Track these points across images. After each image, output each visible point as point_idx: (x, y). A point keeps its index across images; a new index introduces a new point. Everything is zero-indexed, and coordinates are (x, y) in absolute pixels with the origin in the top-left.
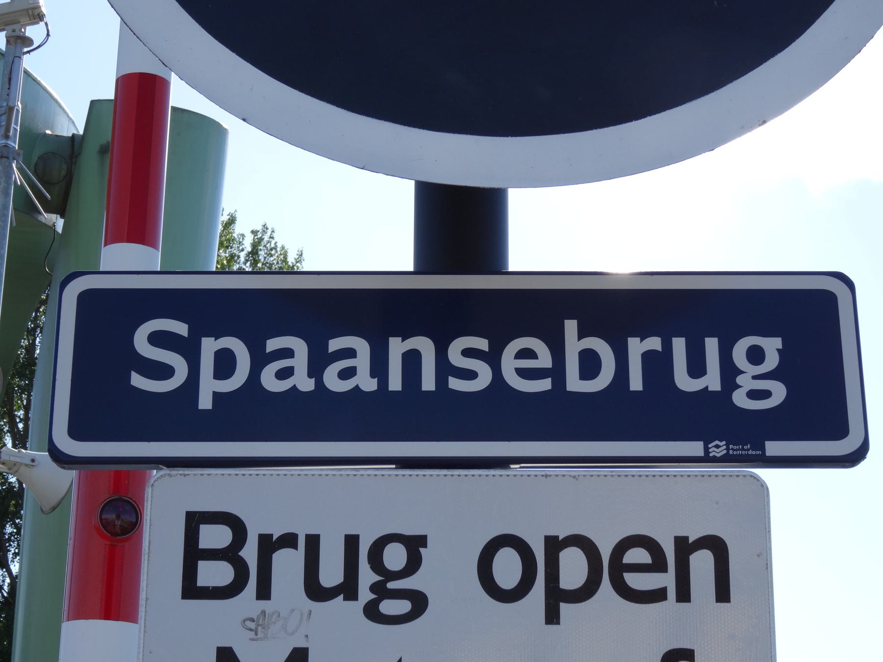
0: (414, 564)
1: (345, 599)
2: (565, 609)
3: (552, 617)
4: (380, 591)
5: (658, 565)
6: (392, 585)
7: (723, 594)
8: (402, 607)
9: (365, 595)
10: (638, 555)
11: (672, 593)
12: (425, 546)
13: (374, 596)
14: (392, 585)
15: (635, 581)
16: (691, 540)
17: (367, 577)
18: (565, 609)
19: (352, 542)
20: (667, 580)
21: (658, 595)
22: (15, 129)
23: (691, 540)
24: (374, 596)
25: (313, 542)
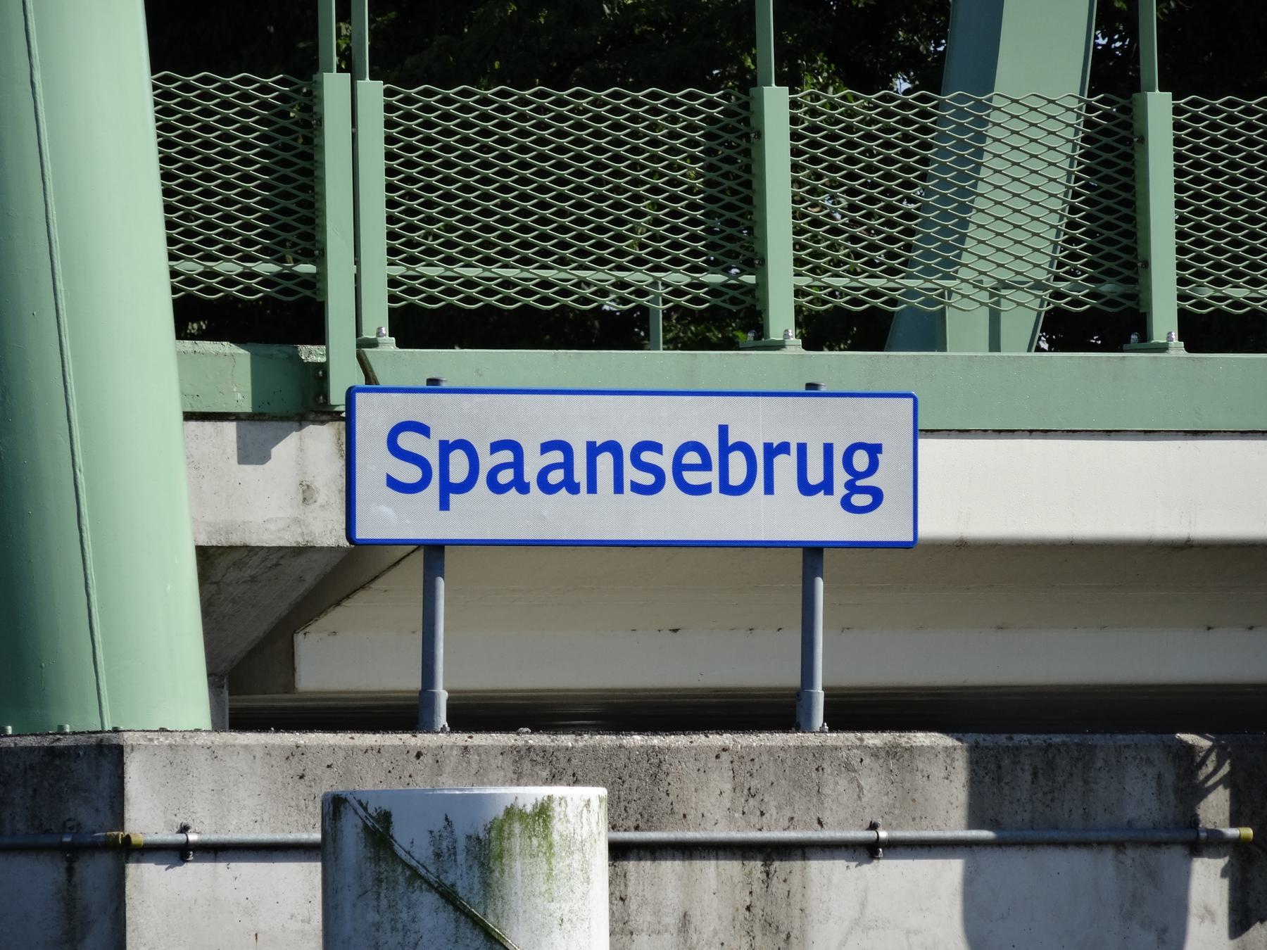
0: (873, 467)
1: (825, 494)
2: (453, 498)
3: (444, 505)
4: (852, 488)
5: (706, 466)
6: (859, 483)
7: (769, 489)
8: (864, 500)
9: (840, 490)
10: (692, 458)
11: (716, 487)
12: (881, 452)
13: (848, 492)
14: (859, 483)
15: (692, 478)
16: (878, 455)
17: (841, 477)
18: (453, 498)
19: (828, 449)
20: (712, 477)
21: (705, 489)
22: (1120, 185)
23: (878, 455)
24: (848, 492)
25: (802, 448)
